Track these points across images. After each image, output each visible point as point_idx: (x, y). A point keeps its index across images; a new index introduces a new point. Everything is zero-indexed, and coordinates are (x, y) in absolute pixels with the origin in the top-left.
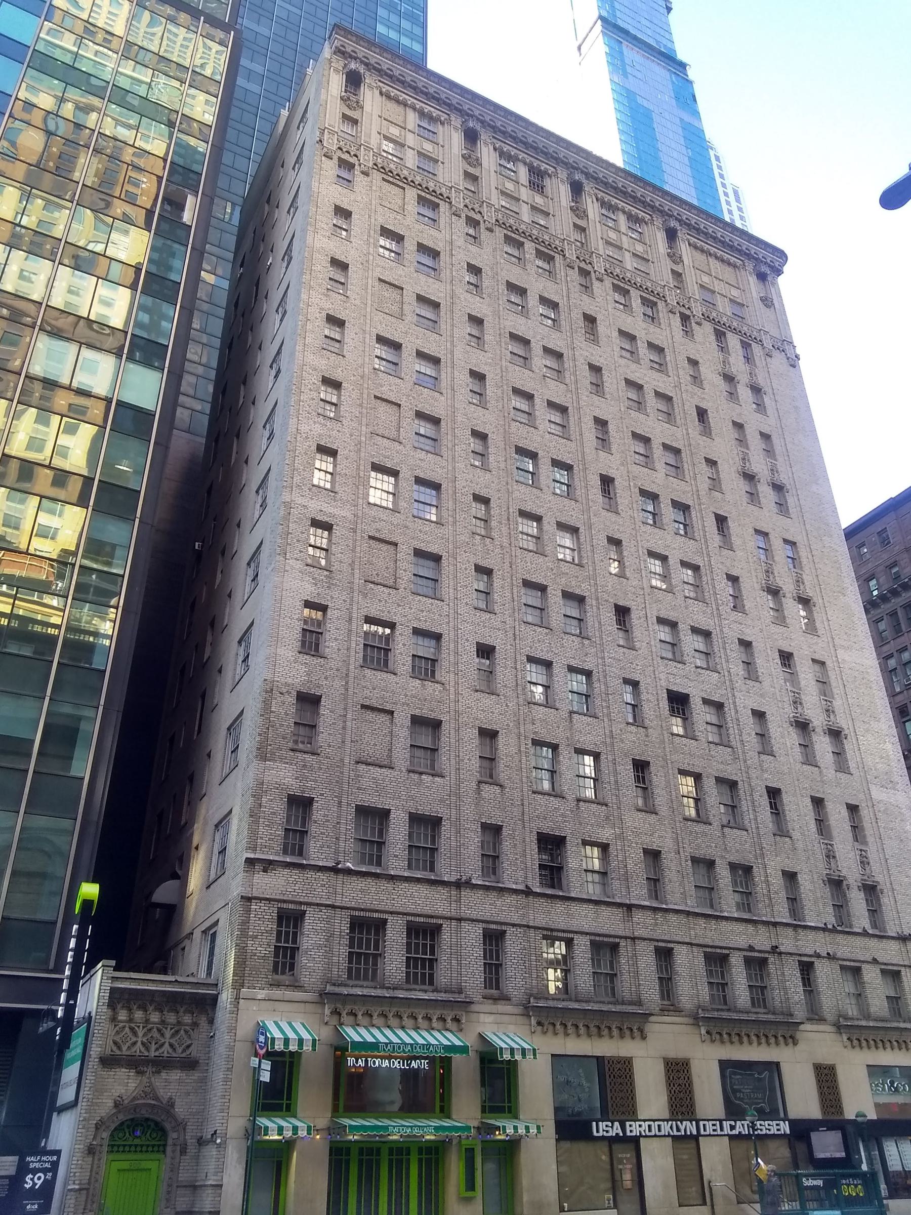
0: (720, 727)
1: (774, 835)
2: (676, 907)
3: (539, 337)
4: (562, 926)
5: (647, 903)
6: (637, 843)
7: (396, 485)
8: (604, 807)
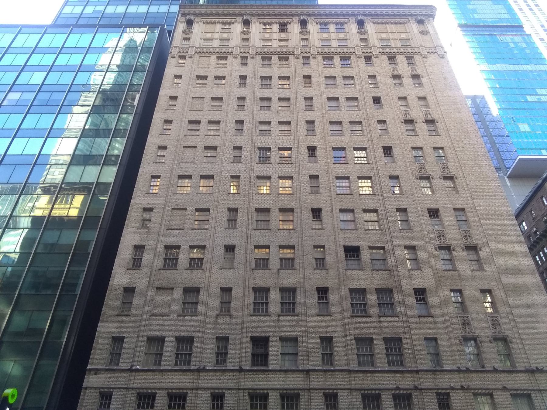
0: (478, 260)
1: (419, 317)
2: (341, 368)
3: (276, 95)
4: (262, 386)
5: (320, 368)
6: (316, 334)
7: (372, 183)
8: (296, 317)
